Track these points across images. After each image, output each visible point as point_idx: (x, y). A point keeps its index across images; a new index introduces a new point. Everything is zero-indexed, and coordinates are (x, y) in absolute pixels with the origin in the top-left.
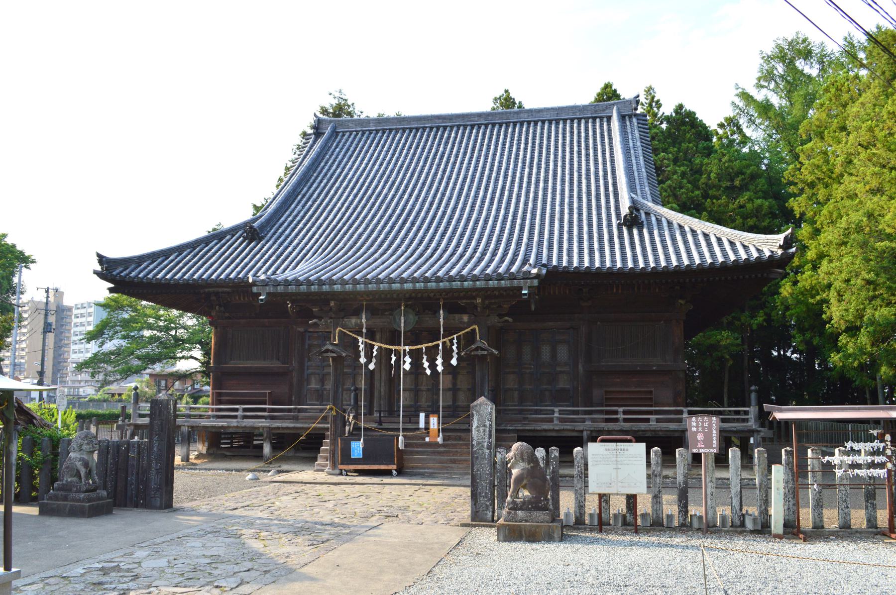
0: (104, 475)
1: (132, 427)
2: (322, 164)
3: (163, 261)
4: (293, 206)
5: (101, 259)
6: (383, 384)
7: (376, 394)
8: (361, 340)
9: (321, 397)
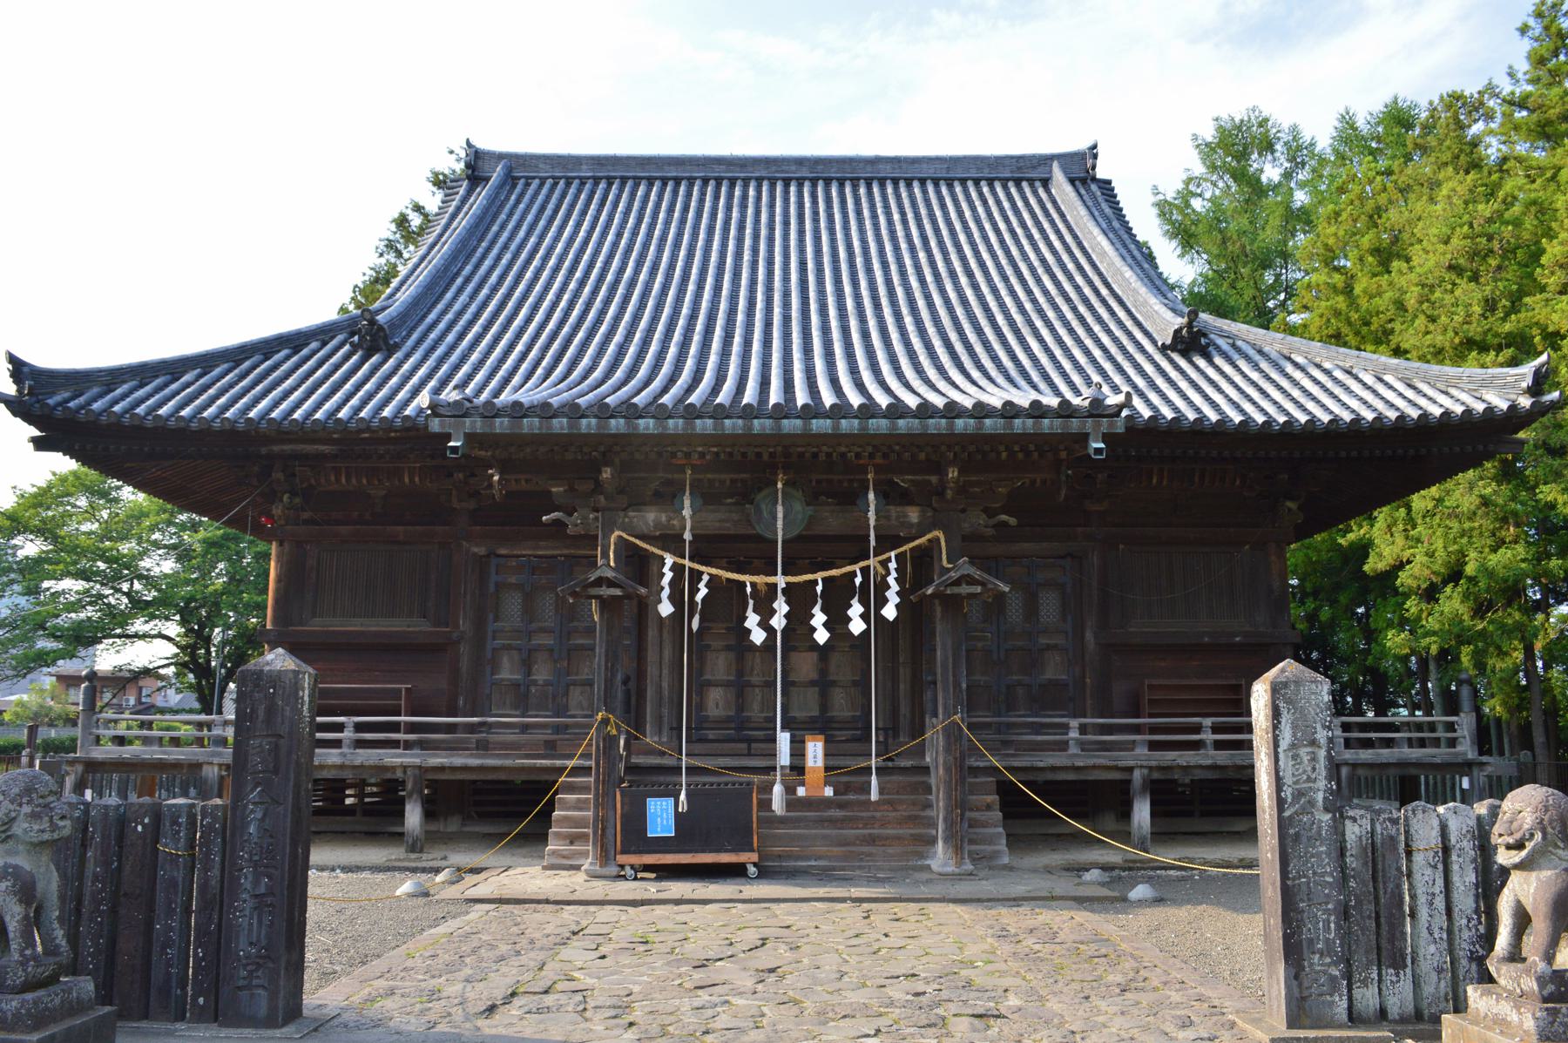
0: (73, 917)
1: (80, 768)
2: (495, 228)
3: (166, 385)
4: (449, 295)
5: (19, 369)
6: (665, 672)
7: (650, 693)
8: (669, 560)
9: (521, 698)
